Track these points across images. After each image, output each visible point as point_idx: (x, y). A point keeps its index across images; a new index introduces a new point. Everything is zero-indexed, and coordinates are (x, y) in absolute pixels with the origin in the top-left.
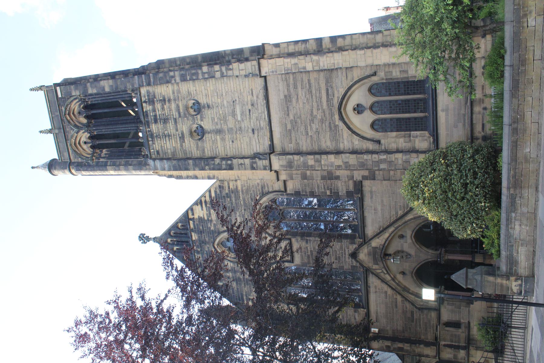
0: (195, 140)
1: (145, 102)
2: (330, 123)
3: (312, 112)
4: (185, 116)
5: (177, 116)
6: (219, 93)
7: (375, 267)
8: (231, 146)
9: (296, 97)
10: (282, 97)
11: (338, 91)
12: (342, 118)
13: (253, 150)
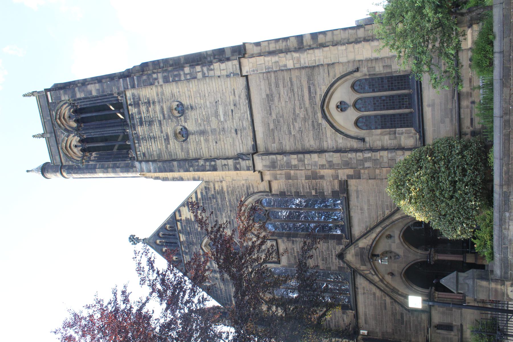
0: (180, 141)
1: (131, 105)
2: (313, 122)
3: (294, 110)
4: (169, 118)
5: (162, 118)
6: (201, 94)
7: (363, 268)
8: (215, 147)
9: (278, 95)
10: (264, 96)
11: (321, 89)
12: (325, 116)
13: (237, 151)
